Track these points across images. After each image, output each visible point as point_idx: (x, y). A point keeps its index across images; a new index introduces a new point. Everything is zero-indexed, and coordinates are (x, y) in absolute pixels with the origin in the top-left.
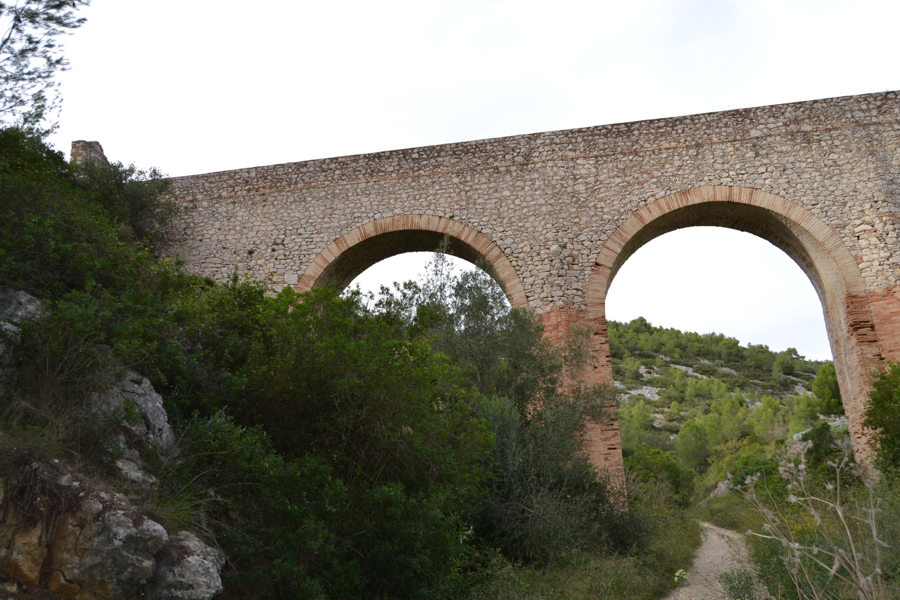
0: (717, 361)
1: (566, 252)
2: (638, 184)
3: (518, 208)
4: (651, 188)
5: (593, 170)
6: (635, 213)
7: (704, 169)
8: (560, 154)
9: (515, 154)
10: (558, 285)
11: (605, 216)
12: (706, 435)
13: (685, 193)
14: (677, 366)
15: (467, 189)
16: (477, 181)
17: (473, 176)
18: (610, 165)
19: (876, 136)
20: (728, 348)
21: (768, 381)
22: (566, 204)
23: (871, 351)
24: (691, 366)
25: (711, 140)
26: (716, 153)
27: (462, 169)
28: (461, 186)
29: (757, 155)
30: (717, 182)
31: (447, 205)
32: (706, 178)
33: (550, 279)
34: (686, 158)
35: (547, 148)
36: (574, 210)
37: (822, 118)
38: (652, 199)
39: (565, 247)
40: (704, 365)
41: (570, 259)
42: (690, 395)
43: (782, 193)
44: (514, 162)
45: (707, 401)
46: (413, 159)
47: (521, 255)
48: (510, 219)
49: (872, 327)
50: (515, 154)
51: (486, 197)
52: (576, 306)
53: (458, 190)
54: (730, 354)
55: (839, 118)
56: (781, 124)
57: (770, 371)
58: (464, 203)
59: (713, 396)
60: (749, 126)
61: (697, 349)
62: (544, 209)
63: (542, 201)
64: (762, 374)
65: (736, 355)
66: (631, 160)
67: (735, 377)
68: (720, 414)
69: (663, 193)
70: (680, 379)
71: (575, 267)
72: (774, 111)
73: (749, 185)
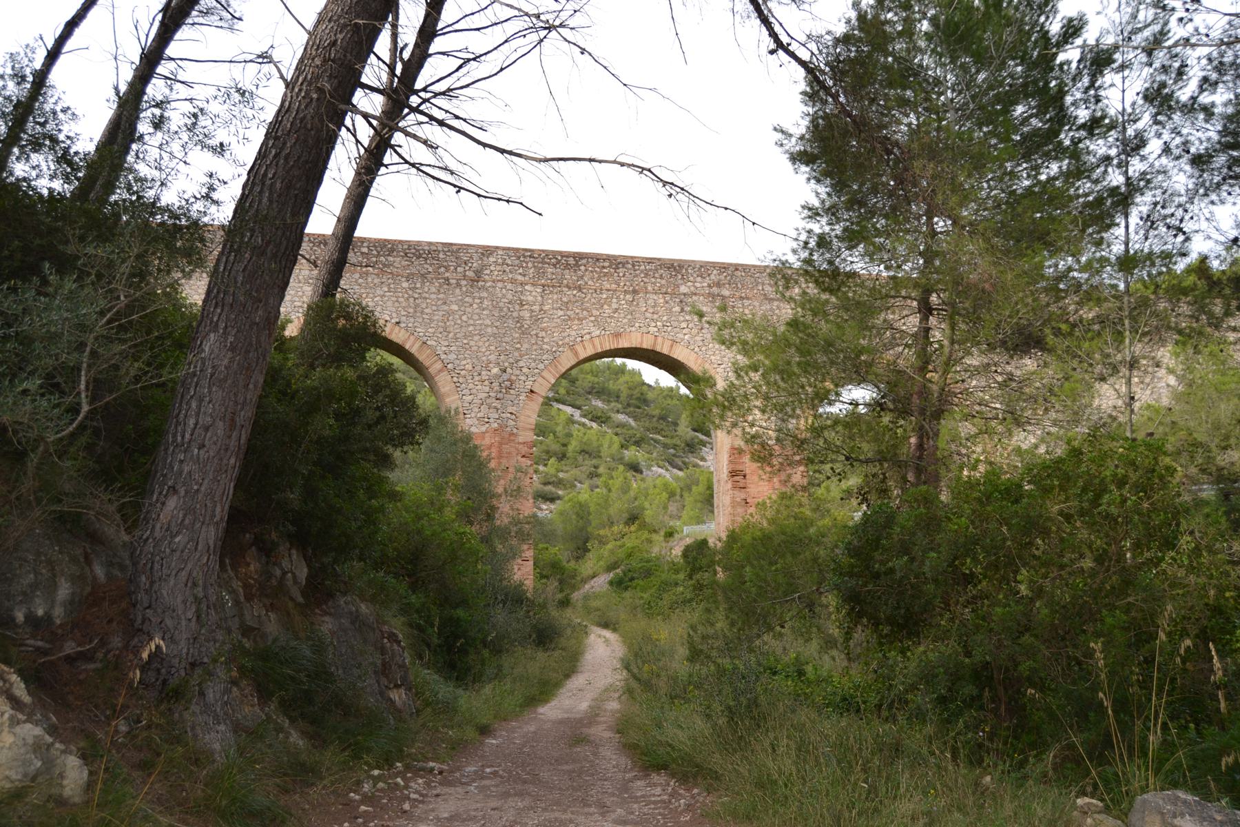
0: (613, 404)
1: (505, 376)
2: (578, 319)
3: (464, 324)
4: (589, 327)
5: (539, 298)
6: (572, 348)
7: (637, 316)
8: (510, 276)
9: (467, 268)
10: (495, 408)
11: (545, 346)
12: (589, 514)
13: (617, 335)
14: (561, 406)
15: (416, 296)
16: (426, 289)
17: (423, 283)
18: (555, 297)
19: (777, 312)
20: (630, 389)
21: (672, 437)
22: (511, 329)
23: (740, 495)
24: (579, 408)
25: (646, 288)
26: (649, 302)
27: (413, 274)
28: (410, 292)
29: (682, 310)
30: (644, 330)
31: (394, 310)
32: (637, 325)
33: (488, 401)
34: (623, 302)
35: (499, 268)
36: (517, 335)
37: (739, 286)
38: (588, 337)
39: (505, 371)
40: (596, 408)
41: (508, 383)
42: (574, 451)
43: (697, 349)
44: (465, 276)
45: (594, 462)
46: (362, 253)
47: (463, 373)
48: (455, 334)
49: (745, 476)
50: (467, 268)
51: (434, 308)
52: (509, 429)
53: (406, 296)
54: (631, 396)
55: (752, 289)
56: (705, 284)
57: (676, 424)
58: (411, 310)
59: (602, 454)
60: (680, 282)
61: (590, 385)
62: (489, 330)
63: (488, 322)
64: (666, 428)
65: (638, 399)
66: (575, 295)
67: (633, 428)
68: (610, 490)
69: (598, 333)
70: (564, 428)
71: (512, 391)
72: (704, 268)
73: (670, 338)
